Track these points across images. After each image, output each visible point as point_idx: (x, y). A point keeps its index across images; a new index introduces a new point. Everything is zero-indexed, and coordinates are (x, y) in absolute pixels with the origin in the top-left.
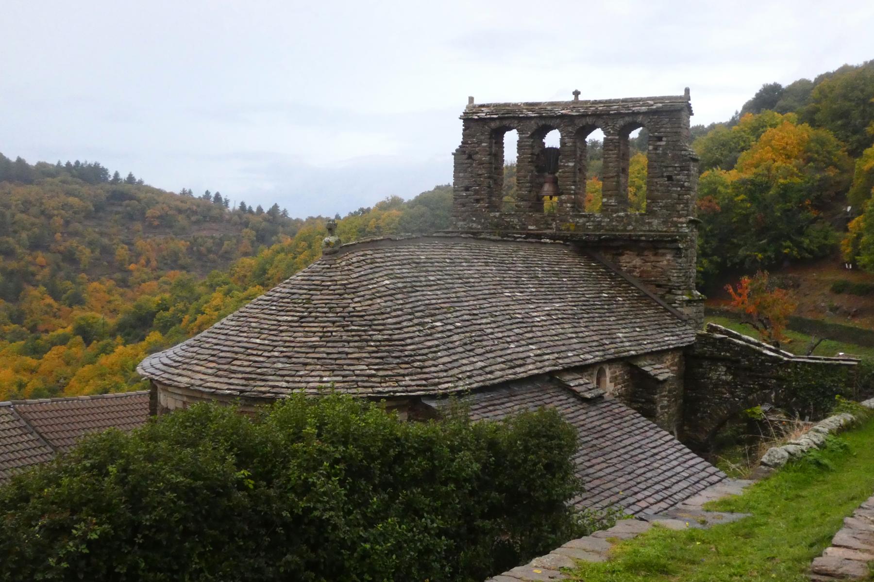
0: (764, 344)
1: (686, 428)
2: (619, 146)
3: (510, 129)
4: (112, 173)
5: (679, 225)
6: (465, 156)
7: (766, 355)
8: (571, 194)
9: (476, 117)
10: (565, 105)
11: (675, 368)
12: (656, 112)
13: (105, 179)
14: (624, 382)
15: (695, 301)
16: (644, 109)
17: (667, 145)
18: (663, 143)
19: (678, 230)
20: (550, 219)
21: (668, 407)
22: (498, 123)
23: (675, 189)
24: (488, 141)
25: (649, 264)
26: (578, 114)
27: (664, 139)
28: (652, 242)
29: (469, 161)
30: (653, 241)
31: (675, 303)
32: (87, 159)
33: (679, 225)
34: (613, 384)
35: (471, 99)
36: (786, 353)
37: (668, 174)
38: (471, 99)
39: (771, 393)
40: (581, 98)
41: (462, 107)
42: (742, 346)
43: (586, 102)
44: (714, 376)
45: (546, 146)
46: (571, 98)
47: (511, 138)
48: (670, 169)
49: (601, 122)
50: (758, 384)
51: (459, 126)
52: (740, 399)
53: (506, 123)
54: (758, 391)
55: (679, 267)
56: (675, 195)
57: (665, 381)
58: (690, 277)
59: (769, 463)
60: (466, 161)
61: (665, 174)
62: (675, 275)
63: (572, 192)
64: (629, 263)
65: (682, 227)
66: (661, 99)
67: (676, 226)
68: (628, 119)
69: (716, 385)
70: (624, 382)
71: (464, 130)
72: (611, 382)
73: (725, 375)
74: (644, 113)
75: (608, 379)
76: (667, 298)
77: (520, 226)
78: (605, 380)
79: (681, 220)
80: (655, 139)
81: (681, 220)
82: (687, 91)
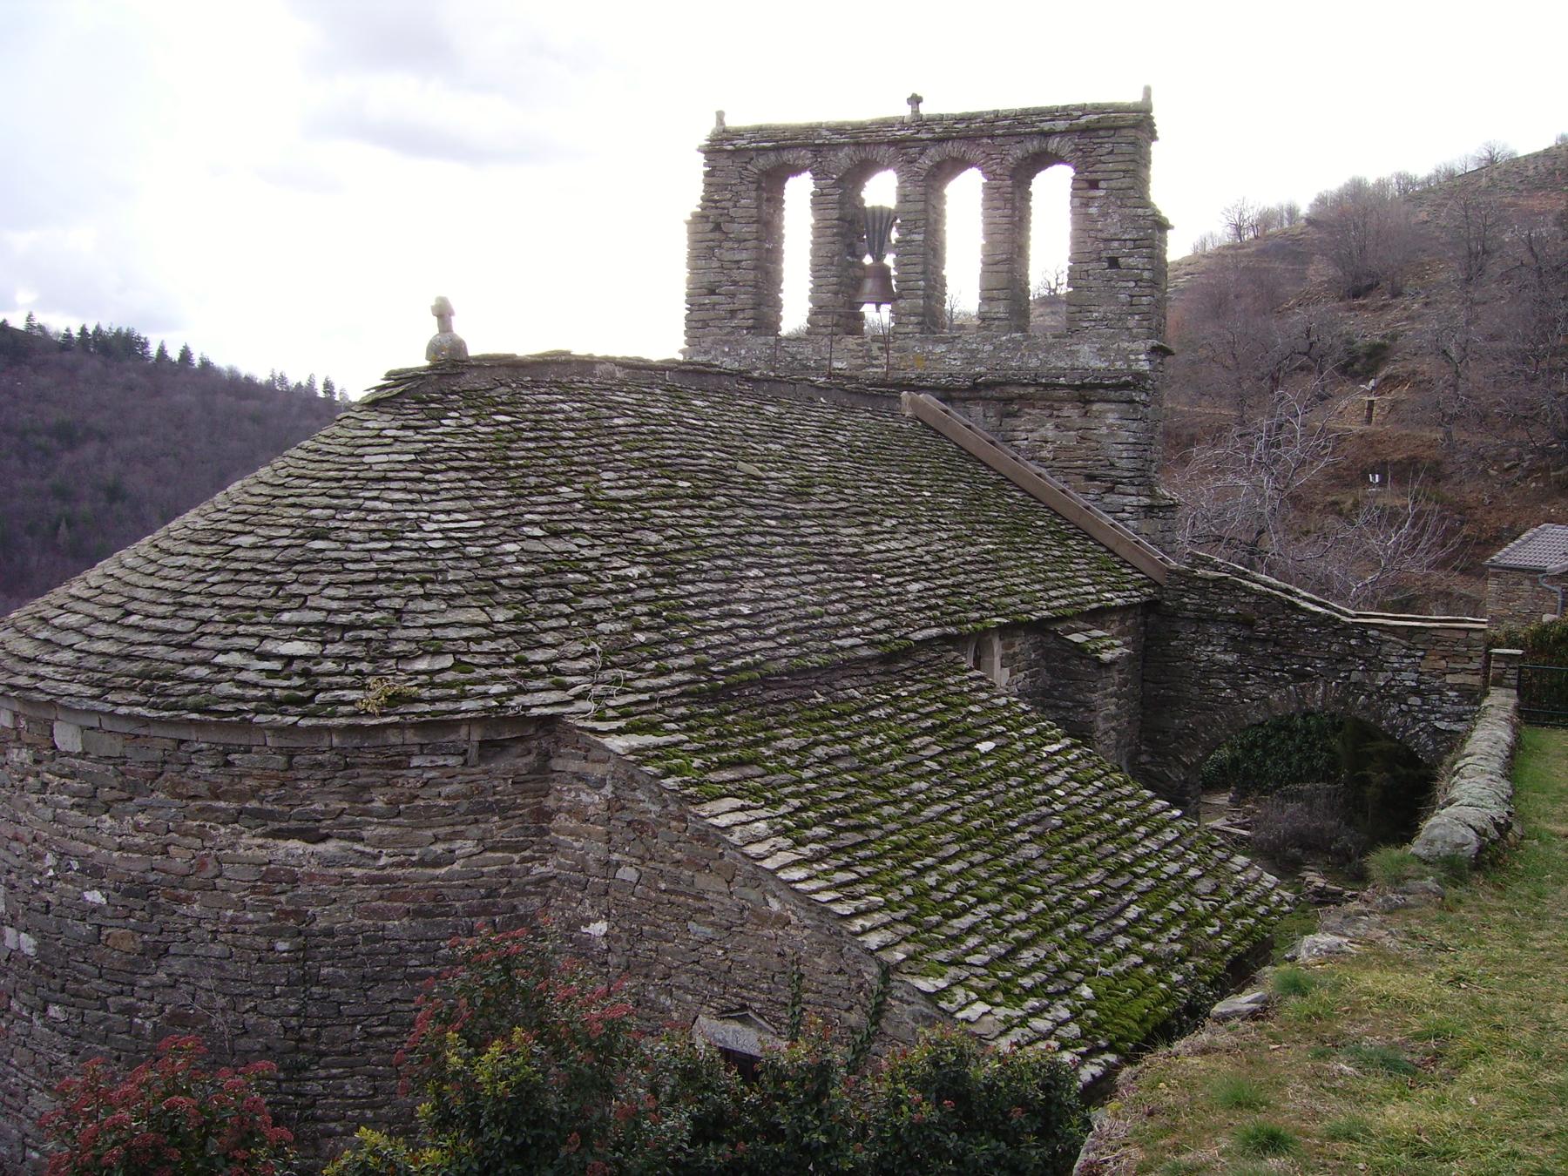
0: (1298, 590)
1: (1144, 758)
2: (1013, 199)
3: (797, 171)
4: (153, 351)
5: (1132, 357)
6: (710, 226)
7: (1304, 610)
8: (917, 297)
9: (730, 147)
10: (903, 124)
11: (1129, 639)
12: (1086, 131)
13: (144, 357)
14: (1029, 667)
15: (1160, 508)
16: (1061, 125)
17: (1107, 197)
18: (1101, 193)
19: (1130, 366)
20: (875, 346)
21: (1114, 717)
22: (772, 156)
23: (1124, 284)
24: (753, 194)
25: (1071, 433)
26: (930, 136)
27: (1102, 184)
28: (1077, 388)
29: (717, 235)
30: (1083, 386)
31: (1123, 511)
32: (109, 320)
33: (1132, 357)
34: (1007, 671)
35: (720, 116)
36: (1319, 609)
37: (1111, 254)
38: (720, 116)
39: (1315, 687)
40: (926, 110)
41: (704, 131)
42: (1259, 594)
43: (940, 119)
44: (1203, 653)
45: (868, 204)
46: (906, 111)
47: (799, 192)
48: (1115, 244)
49: (975, 153)
50: (1290, 672)
51: (697, 166)
52: (1253, 700)
53: (788, 156)
54: (1289, 683)
55: (1131, 440)
56: (1123, 297)
57: (1113, 663)
58: (1152, 461)
59: (1431, 860)
60: (711, 236)
61: (1104, 254)
62: (1125, 454)
63: (920, 292)
64: (1032, 431)
65: (1138, 360)
66: (1098, 109)
67: (1127, 360)
68: (1033, 146)
69: (1207, 674)
70: (1029, 667)
71: (707, 174)
72: (1002, 666)
73: (1225, 651)
74: (1062, 133)
75: (997, 660)
76: (1107, 500)
77: (815, 361)
78: (992, 663)
79: (1134, 346)
80: (1086, 185)
81: (1134, 346)
82: (1147, 92)
